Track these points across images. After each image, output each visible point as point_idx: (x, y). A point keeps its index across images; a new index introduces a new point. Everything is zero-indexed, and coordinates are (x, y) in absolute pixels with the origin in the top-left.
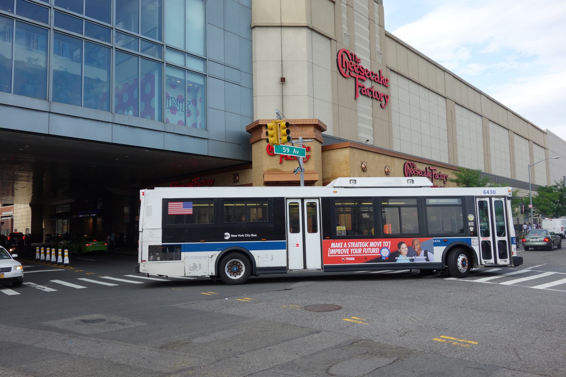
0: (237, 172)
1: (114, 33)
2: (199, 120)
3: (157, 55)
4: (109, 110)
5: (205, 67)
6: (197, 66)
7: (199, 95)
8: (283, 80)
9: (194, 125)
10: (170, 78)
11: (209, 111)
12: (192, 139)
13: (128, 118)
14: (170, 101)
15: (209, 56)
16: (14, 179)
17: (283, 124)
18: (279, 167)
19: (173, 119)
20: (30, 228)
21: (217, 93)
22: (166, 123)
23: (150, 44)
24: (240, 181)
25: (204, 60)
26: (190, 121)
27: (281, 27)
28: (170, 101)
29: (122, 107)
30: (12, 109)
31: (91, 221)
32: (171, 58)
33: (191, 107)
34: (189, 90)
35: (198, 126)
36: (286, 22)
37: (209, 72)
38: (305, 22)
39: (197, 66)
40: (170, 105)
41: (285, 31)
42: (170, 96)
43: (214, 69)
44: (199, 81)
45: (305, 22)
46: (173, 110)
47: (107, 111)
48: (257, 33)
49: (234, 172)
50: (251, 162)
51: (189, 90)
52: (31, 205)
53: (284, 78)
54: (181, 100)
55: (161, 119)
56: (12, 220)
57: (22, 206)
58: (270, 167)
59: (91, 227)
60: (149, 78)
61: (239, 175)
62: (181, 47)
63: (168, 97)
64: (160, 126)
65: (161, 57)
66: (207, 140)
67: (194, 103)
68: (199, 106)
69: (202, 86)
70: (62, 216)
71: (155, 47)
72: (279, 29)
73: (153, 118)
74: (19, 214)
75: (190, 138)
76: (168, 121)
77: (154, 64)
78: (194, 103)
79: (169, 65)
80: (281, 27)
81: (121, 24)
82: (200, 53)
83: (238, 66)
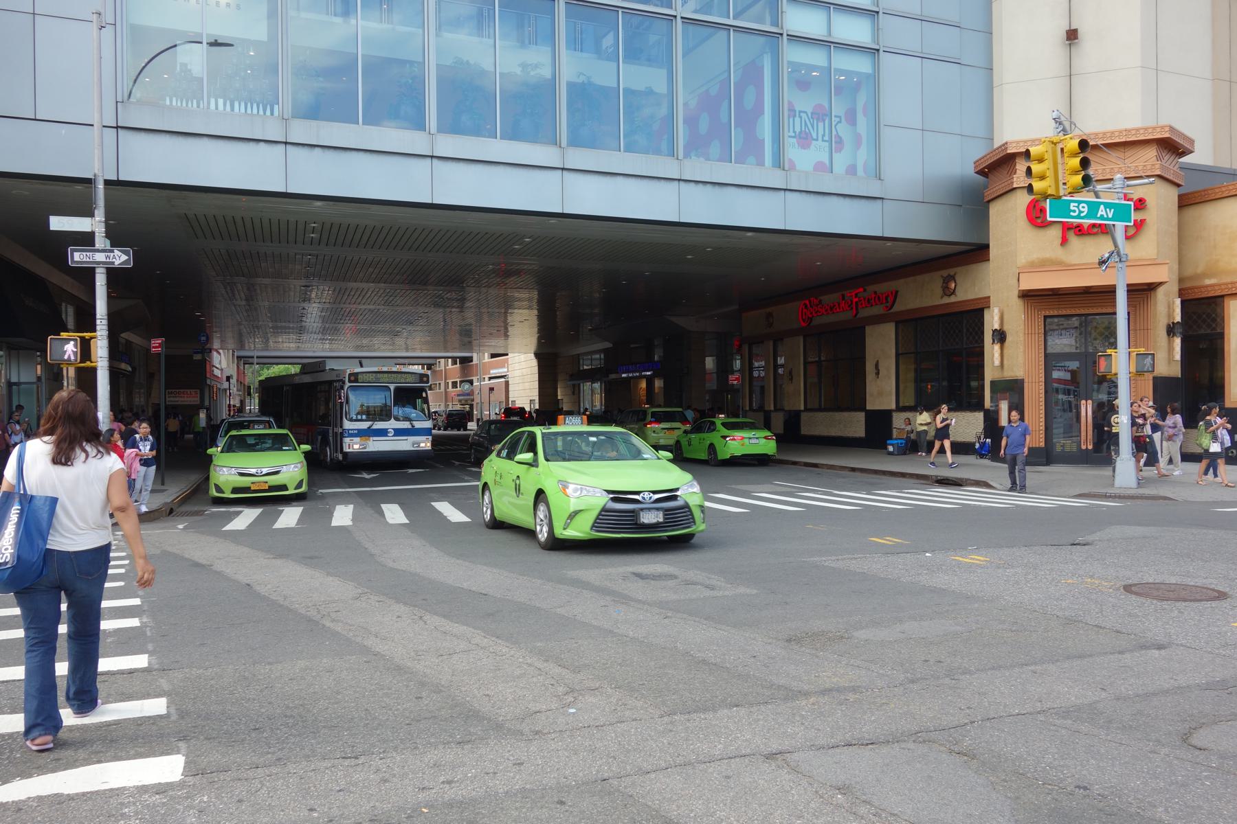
0: (951, 271)
2: (863, 156)
5: (876, 31)
7: (862, 98)
8: (1072, 35)
9: (852, 170)
11: (886, 133)
12: (847, 201)
16: (507, 306)
26: (841, 162)
31: (643, 385)
33: (843, 130)
34: (839, 90)
35: (860, 172)
37: (887, 41)
40: (798, 129)
42: (797, 109)
43: (897, 33)
44: (861, 65)
46: (805, 140)
49: (945, 273)
50: (987, 247)
52: (537, 355)
54: (821, 114)
55: (779, 163)
56: (507, 383)
57: (523, 357)
58: (1036, 256)
61: (957, 278)
63: (792, 110)
64: (776, 179)
65: (775, 23)
66: (879, 202)
67: (851, 118)
69: (868, 76)
70: (591, 376)
73: (761, 163)
74: (517, 373)
75: (841, 200)
77: (762, 40)
79: (793, 38)
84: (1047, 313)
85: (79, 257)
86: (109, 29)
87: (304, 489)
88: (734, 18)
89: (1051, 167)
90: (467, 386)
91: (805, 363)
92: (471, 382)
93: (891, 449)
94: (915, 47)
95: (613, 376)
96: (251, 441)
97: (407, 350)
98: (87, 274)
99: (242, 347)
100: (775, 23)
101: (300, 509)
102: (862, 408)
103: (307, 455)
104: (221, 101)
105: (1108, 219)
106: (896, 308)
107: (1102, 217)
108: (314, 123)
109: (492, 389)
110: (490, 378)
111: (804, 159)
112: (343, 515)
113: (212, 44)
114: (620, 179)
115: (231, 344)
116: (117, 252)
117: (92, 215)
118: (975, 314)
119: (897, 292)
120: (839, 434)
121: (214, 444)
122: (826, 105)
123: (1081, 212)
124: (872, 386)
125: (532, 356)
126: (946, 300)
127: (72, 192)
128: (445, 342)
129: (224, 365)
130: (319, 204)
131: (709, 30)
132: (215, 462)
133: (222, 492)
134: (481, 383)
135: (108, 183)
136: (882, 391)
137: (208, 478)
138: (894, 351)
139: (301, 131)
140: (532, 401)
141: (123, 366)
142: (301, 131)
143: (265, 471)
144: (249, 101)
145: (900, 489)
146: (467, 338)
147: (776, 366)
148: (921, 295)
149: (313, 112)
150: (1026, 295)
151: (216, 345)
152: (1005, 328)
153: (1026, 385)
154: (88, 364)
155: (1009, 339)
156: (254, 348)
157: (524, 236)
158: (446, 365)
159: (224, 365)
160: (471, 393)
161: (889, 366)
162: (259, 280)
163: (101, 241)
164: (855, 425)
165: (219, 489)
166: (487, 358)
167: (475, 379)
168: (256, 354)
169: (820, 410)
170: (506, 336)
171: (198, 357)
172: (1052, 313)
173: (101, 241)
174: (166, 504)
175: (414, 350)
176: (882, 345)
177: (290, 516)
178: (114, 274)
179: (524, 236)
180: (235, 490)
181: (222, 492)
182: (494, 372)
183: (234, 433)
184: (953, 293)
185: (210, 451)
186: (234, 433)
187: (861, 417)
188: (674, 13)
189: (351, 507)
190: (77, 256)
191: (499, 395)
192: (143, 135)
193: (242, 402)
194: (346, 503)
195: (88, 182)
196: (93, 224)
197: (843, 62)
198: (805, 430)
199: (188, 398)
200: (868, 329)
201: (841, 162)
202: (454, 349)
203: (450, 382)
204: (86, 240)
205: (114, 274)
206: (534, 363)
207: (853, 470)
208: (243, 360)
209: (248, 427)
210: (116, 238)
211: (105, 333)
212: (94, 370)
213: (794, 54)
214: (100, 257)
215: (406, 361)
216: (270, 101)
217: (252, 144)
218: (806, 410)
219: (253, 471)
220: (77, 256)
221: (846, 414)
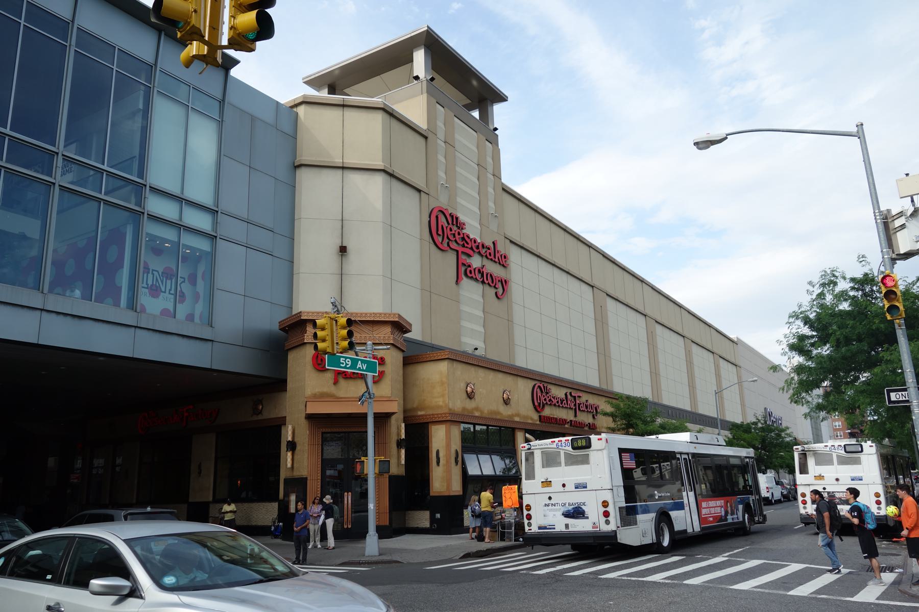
1: (59, 161)
3: (133, 200)
5: (215, 224)
6: (202, 221)
7: (202, 268)
8: (343, 250)
9: (190, 318)
10: (153, 238)
11: (218, 294)
13: (74, 301)
14: (150, 276)
15: (224, 206)
17: (343, 321)
18: (332, 389)
21: (232, 267)
22: (141, 312)
23: (123, 183)
25: (213, 212)
26: (182, 311)
27: (343, 168)
28: (150, 276)
29: (61, 283)
33: (186, 288)
35: (197, 320)
39: (202, 221)
40: (150, 283)
42: (151, 267)
43: (228, 227)
44: (204, 245)
46: (155, 291)
50: (285, 381)
51: (185, 259)
53: (345, 247)
54: (169, 274)
58: (317, 390)
60: (115, 237)
63: (147, 269)
64: (128, 318)
65: (139, 204)
67: (193, 280)
68: (201, 286)
69: (207, 253)
71: (130, 187)
73: (117, 304)
75: (181, 340)
76: (143, 310)
77: (127, 214)
83: (270, 225)
88: (106, 194)
107: (359, 369)
126: (255, 418)
131: (83, 199)
152: (296, 440)
155: (298, 448)
172: (327, 430)
176: (205, 453)
184: (260, 412)
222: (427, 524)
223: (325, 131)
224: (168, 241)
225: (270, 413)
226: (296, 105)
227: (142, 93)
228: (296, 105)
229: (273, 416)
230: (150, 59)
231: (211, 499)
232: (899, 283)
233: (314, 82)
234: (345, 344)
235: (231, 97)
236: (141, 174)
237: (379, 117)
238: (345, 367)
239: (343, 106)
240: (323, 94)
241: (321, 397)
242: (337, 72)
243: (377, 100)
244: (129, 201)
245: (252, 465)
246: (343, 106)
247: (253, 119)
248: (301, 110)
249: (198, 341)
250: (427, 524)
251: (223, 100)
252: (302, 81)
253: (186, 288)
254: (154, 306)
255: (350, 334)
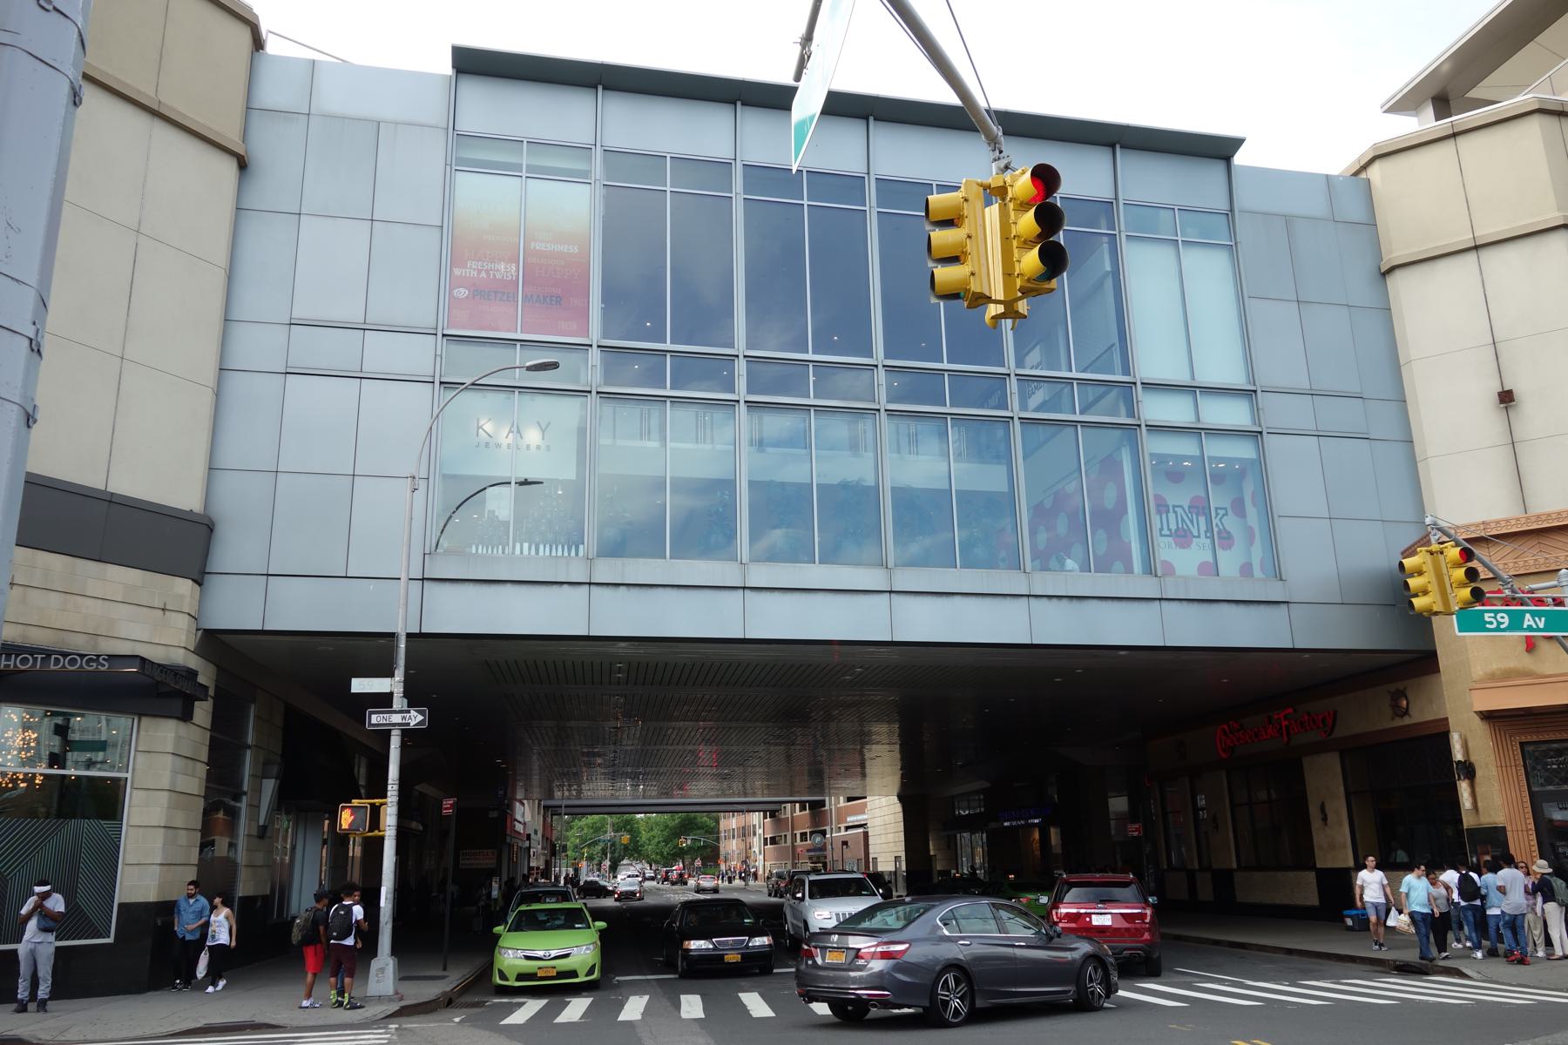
0: (1400, 685)
1: (1013, 385)
2: (1257, 554)
3: (1123, 410)
4: (1017, 566)
5: (1256, 412)
6: (1234, 414)
7: (1249, 488)
8: (1506, 397)
9: (1246, 570)
10: (1161, 459)
11: (1281, 525)
12: (1242, 608)
13: (1072, 578)
14: (1172, 516)
15: (1263, 380)
16: (864, 739)
17: (1454, 553)
18: (1526, 662)
19: (1185, 561)
20: (903, 855)
21: (1297, 475)
22: (1164, 575)
23: (1103, 389)
24: (1414, 711)
25: (1249, 394)
26: (1229, 562)
27: (1476, 248)
28: (1172, 516)
29: (1047, 559)
30: (820, 596)
31: (1037, 835)
32: (1155, 409)
33: (1231, 523)
34: (1218, 478)
35: (1257, 573)
36: (1486, 232)
37: (1268, 422)
38: (1557, 214)
39: (1234, 414)
40: (1173, 527)
41: (1491, 257)
42: (1170, 503)
43: (1278, 412)
44: (1243, 450)
45: (1557, 214)
46: (1183, 537)
47: (1010, 568)
48: (1400, 284)
49: (1393, 687)
50: (1435, 653)
51: (1218, 478)
52: (900, 798)
53: (1510, 393)
54: (1200, 507)
55: (1149, 570)
56: (866, 835)
57: (884, 800)
58: (1495, 666)
59: (1038, 853)
60: (1110, 466)
61: (1408, 693)
62: (1182, 378)
63: (1163, 507)
64: (1148, 588)
65: (1131, 414)
66: (1284, 607)
67: (1239, 508)
68: (1253, 515)
69: (1252, 462)
70: (971, 824)
71: (1114, 393)
72: (1472, 256)
73: (1129, 570)
74: (878, 821)
75: (1233, 608)
76: (1169, 570)
77: (1117, 433)
78: (1239, 508)
79: (1154, 428)
80: (1476, 248)
81: (1035, 356)
82: (1238, 379)
83: (1354, 388)
84: (1524, 739)
85: (376, 719)
86: (422, 485)
87: (595, 976)
88: (1082, 413)
89: (1434, 580)
90: (818, 839)
91: (1233, 806)
92: (824, 833)
93: (1349, 922)
94: (1310, 425)
95: (993, 825)
96: (542, 917)
97: (746, 795)
98: (385, 735)
99: (551, 796)
100: (1131, 414)
101: (589, 1000)
102: (1313, 867)
103: (602, 932)
104: (526, 545)
105: (1538, 630)
106: (1338, 733)
107: (1530, 628)
108: (619, 561)
109: (845, 843)
110: (847, 828)
111: (1185, 561)
112: (634, 1008)
113: (521, 484)
114: (957, 599)
115: (536, 793)
116: (413, 713)
117: (391, 675)
118: (1439, 736)
119: (1335, 713)
120: (1285, 901)
121: (502, 920)
122: (1202, 494)
123: (1499, 624)
124: (1320, 837)
125: (895, 799)
126: (1399, 722)
127: (371, 651)
128: (792, 784)
129: (528, 818)
130: (623, 644)
131: (1053, 429)
132: (501, 943)
133: (506, 979)
134: (836, 834)
135: (409, 635)
136: (1333, 840)
137: (490, 965)
138: (1342, 788)
139: (606, 570)
140: (897, 858)
141: (414, 825)
142: (606, 570)
143: (554, 953)
144: (554, 543)
145: (1336, 978)
146: (818, 780)
147: (1196, 810)
148: (1368, 717)
149: (614, 549)
150: (1488, 716)
151: (519, 796)
152: (1473, 759)
153: (1509, 834)
154: (376, 833)
155: (1479, 773)
156: (560, 796)
157: (854, 667)
158: (793, 811)
159: (528, 818)
160: (823, 848)
161: (1338, 808)
162: (573, 724)
163: (399, 702)
164: (1306, 891)
165: (503, 976)
166: (842, 803)
167: (828, 828)
168: (565, 802)
169: (1260, 868)
170: (864, 775)
171: (494, 814)
172: (1529, 739)
173: (399, 702)
174: (445, 993)
175: (754, 794)
176: (1326, 783)
177: (575, 1009)
178: (407, 734)
179: (854, 667)
180: (520, 977)
181: (506, 979)
182: (852, 820)
183: (523, 908)
184: (1406, 712)
185: (498, 929)
186: (523, 908)
187: (1311, 877)
188: (1009, 414)
189: (646, 998)
190: (375, 719)
191: (856, 851)
192: (447, 586)
193: (548, 863)
194: (641, 993)
195: (392, 635)
196: (391, 685)
197: (1217, 449)
198: (1241, 897)
199: (485, 860)
200: (1306, 761)
201: (1229, 562)
202: (799, 793)
203: (798, 833)
204: (384, 701)
205: (407, 734)
206: (898, 808)
207: (1290, 952)
208: (550, 811)
209: (538, 901)
210: (414, 696)
211: (395, 799)
212: (382, 839)
213: (1155, 445)
214: (396, 718)
215: (744, 807)
216: (575, 541)
217: (555, 588)
218: (1240, 868)
219: (540, 954)
220: (375, 719)
221: (1291, 874)
222: (1313, 900)
223: (1419, 203)
224: (1186, 458)
225: (1421, 713)
226: (1364, 167)
227: (1106, 246)
228: (1364, 167)
229: (1429, 717)
230: (1105, 193)
231: (1235, 866)
232: (644, 836)
233: (1404, 104)
234: (1466, 593)
235: (1246, 197)
236: (1126, 370)
237: (1535, 123)
238: (1498, 629)
239: (1454, 135)
240: (1423, 123)
241: (1505, 677)
242: (1446, 67)
243: (1523, 100)
244: (1115, 413)
245: (1415, 807)
246: (1454, 135)
247: (1288, 220)
248: (1374, 173)
249: (1262, 607)
250: (1313, 900)
251: (1232, 210)
252: (1380, 111)
253: (1231, 523)
254: (1185, 561)
255: (1472, 574)
